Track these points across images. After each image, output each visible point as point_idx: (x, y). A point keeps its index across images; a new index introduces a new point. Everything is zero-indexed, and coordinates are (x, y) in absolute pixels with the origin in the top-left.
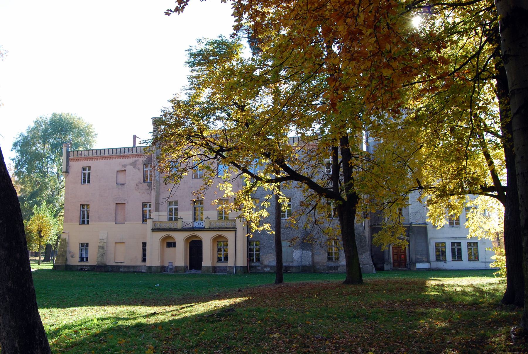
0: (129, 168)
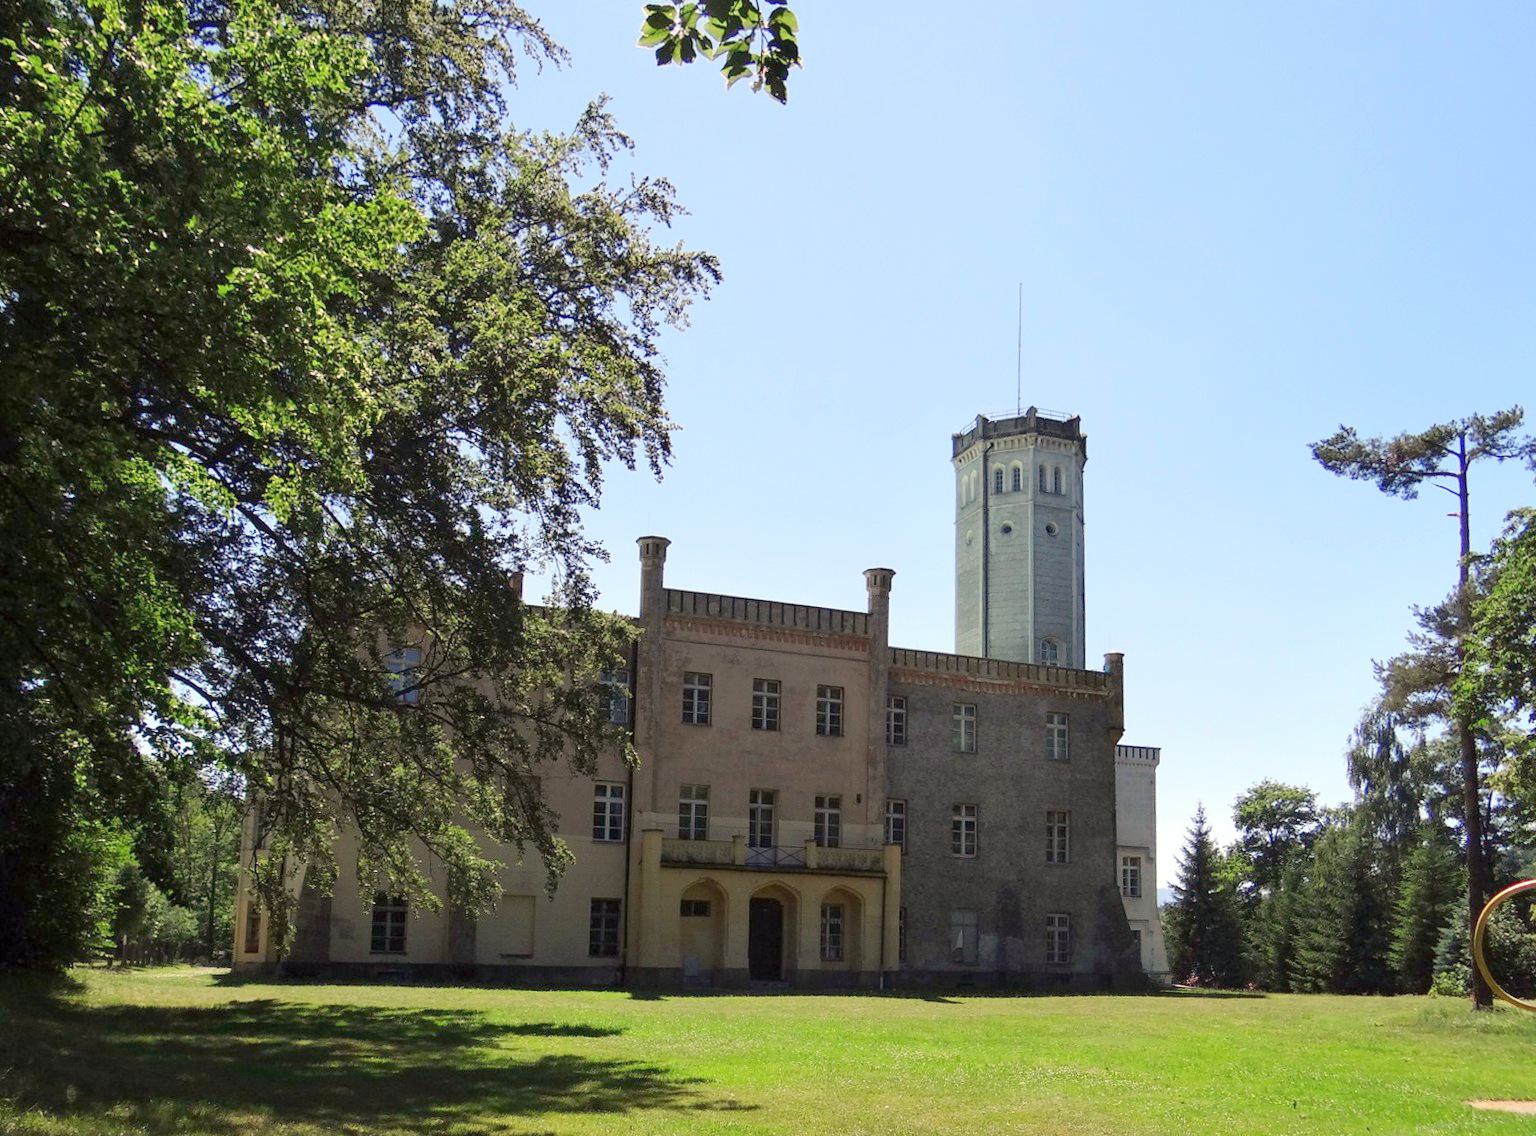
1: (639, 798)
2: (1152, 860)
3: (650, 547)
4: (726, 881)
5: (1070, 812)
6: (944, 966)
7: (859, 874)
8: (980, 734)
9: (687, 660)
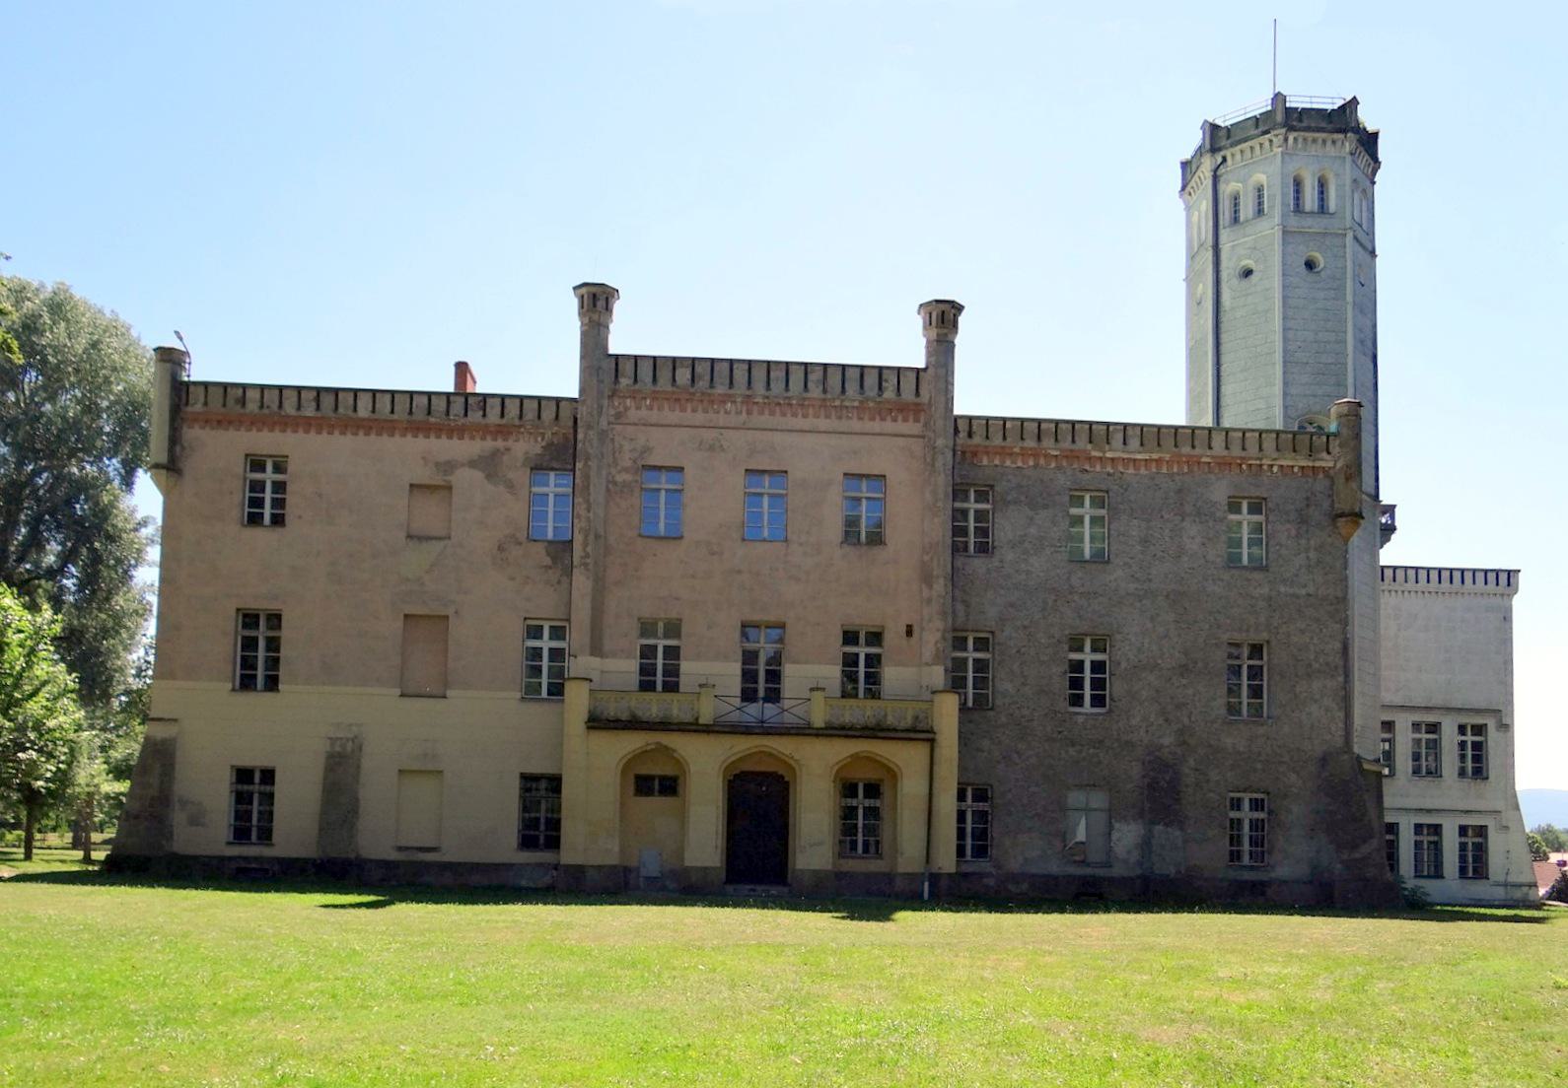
0: (466, 479)
1: (578, 636)
2: (1506, 727)
3: (586, 297)
4: (687, 747)
5: (1268, 642)
6: (1054, 868)
7: (892, 735)
8: (1112, 532)
9: (646, 450)
